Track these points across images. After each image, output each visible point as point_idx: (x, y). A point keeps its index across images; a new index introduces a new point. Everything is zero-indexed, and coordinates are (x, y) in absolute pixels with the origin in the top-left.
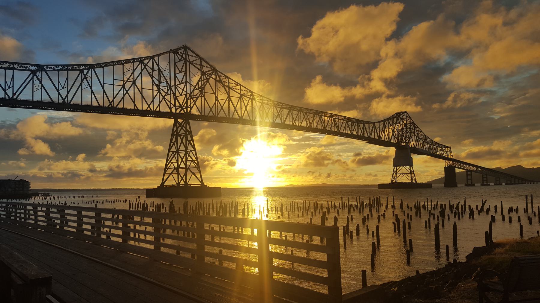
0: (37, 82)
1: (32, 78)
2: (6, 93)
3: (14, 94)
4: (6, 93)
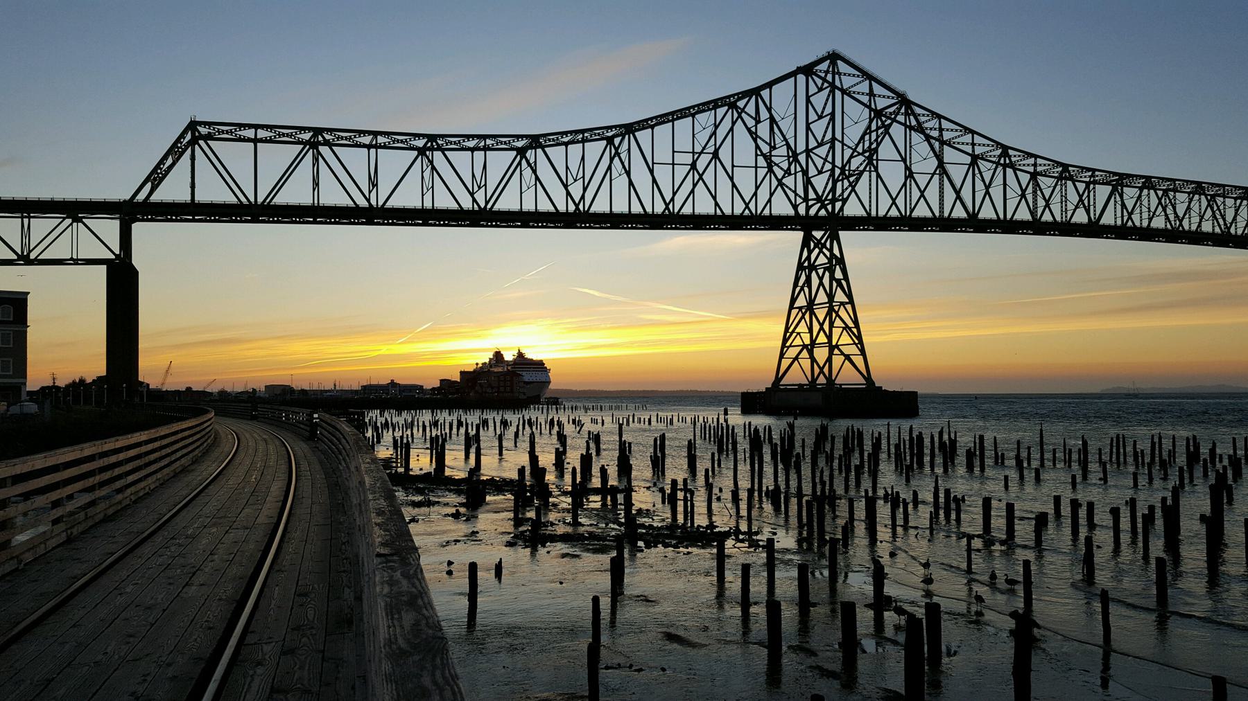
0: (528, 172)
1: (520, 163)
2: (474, 200)
3: (487, 203)
4: (474, 200)
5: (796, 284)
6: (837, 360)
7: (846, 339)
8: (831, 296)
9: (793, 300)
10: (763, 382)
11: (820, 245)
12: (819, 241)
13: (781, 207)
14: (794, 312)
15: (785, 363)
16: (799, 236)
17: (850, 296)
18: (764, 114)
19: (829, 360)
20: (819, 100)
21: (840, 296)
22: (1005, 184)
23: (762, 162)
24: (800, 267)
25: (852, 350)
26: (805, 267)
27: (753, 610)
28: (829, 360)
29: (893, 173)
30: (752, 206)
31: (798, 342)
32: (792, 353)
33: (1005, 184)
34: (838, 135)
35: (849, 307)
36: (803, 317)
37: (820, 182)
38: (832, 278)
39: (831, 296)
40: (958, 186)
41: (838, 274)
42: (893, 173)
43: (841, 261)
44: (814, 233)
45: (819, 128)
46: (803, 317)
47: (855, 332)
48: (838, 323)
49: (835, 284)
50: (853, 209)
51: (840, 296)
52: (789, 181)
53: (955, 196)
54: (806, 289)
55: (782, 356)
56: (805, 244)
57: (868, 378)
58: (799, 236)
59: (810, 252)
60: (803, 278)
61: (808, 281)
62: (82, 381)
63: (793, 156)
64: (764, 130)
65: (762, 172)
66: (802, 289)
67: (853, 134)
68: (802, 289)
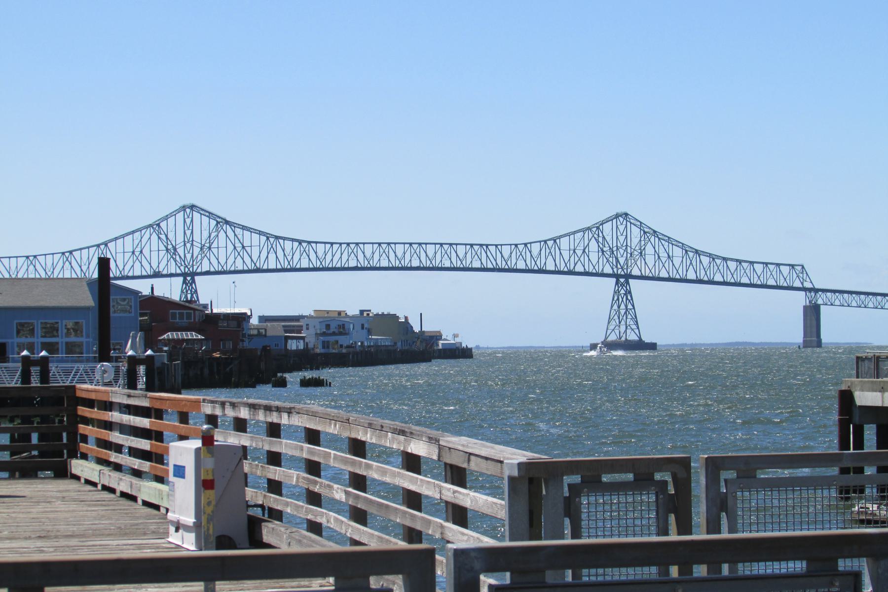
6: (629, 331)
7: (632, 323)
8: (626, 306)
9: (612, 307)
11: (622, 285)
13: (608, 270)
15: (609, 332)
17: (633, 306)
18: (601, 235)
19: (626, 331)
20: (622, 228)
21: (630, 306)
24: (615, 292)
25: (634, 327)
27: (275, 414)
28: (626, 331)
29: (650, 260)
34: (629, 244)
37: (622, 260)
38: (627, 299)
39: (626, 306)
41: (629, 298)
42: (650, 260)
43: (630, 292)
45: (622, 239)
48: (629, 316)
51: (630, 306)
52: (611, 259)
56: (617, 283)
57: (640, 338)
58: (614, 280)
61: (618, 299)
62: (395, 317)
63: (611, 249)
64: (601, 239)
67: (635, 241)
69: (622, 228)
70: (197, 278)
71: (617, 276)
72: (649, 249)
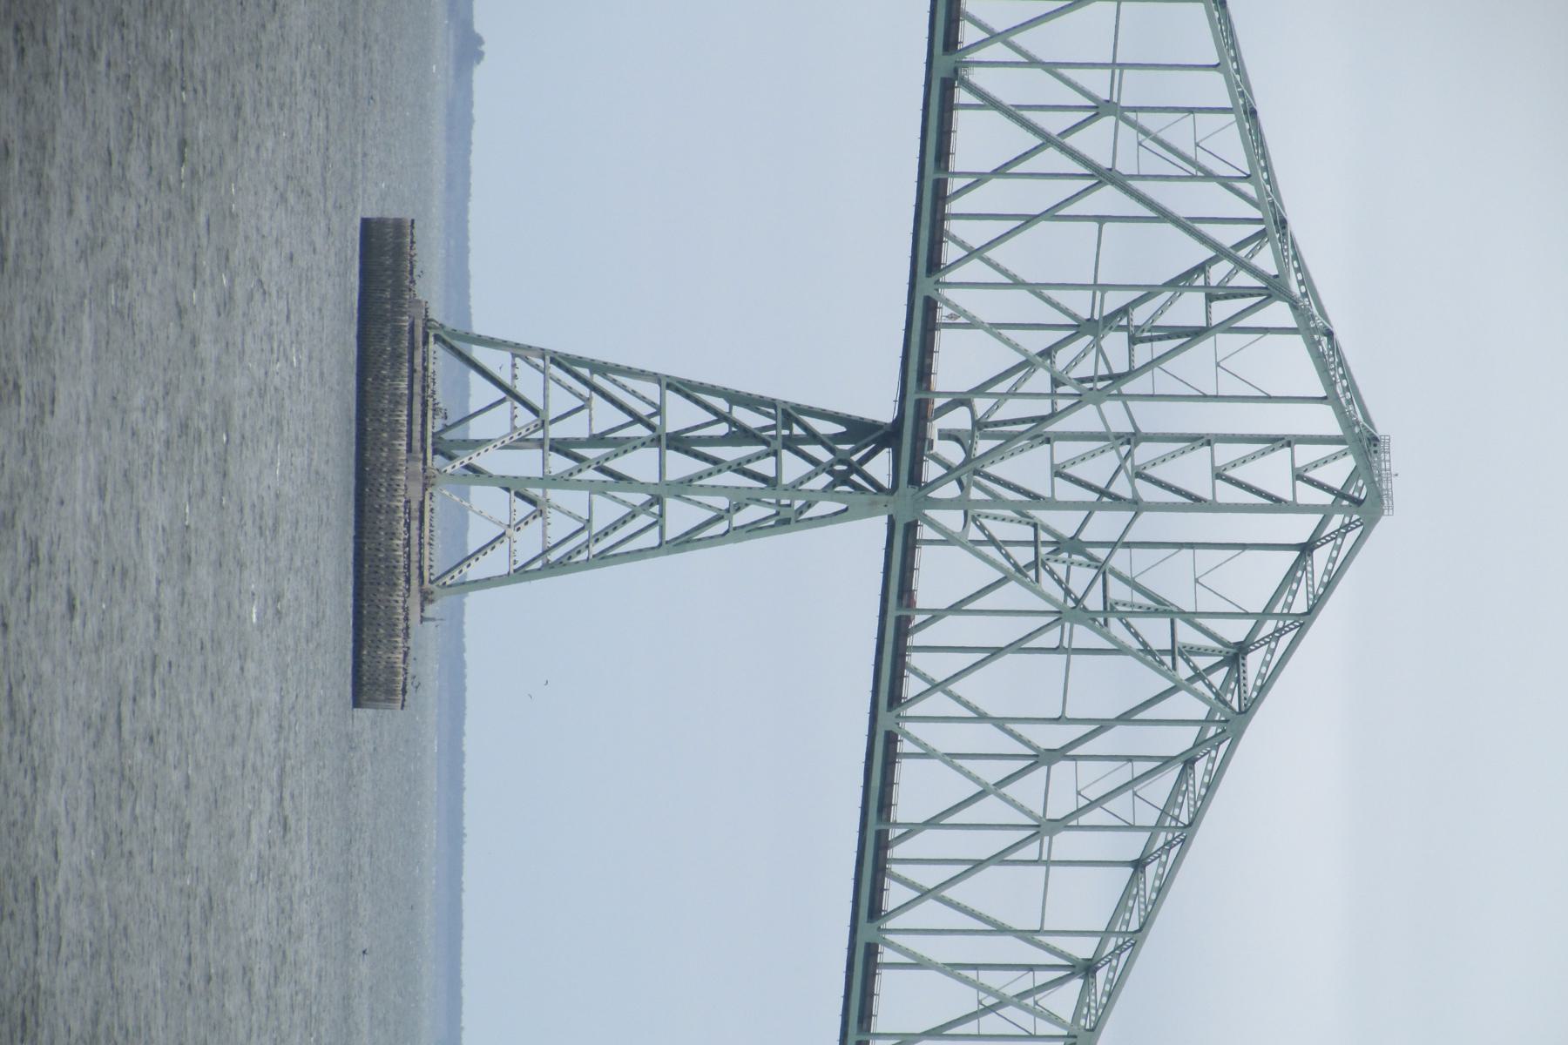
5: (735, 398)
9: (687, 389)
10: (430, 291)
12: (856, 468)
13: (960, 361)
14: (651, 390)
16: (885, 413)
17: (686, 541)
22: (1031, 968)
23: (1114, 301)
26: (789, 424)
30: (997, 51)
31: (560, 401)
32: (529, 383)
33: (1031, 968)
35: (651, 538)
36: (637, 419)
37: (1027, 468)
40: (948, 893)
43: (784, 521)
44: (885, 456)
46: (637, 419)
47: (587, 554)
49: (722, 503)
50: (941, 574)
53: (999, 28)
54: (722, 429)
55: (519, 351)
59: (828, 442)
60: (752, 420)
65: (1081, 305)
66: (721, 417)
68: (721, 417)
69: (1272, 472)
70: (871, 532)
71: (904, 435)
72: (1109, 683)
